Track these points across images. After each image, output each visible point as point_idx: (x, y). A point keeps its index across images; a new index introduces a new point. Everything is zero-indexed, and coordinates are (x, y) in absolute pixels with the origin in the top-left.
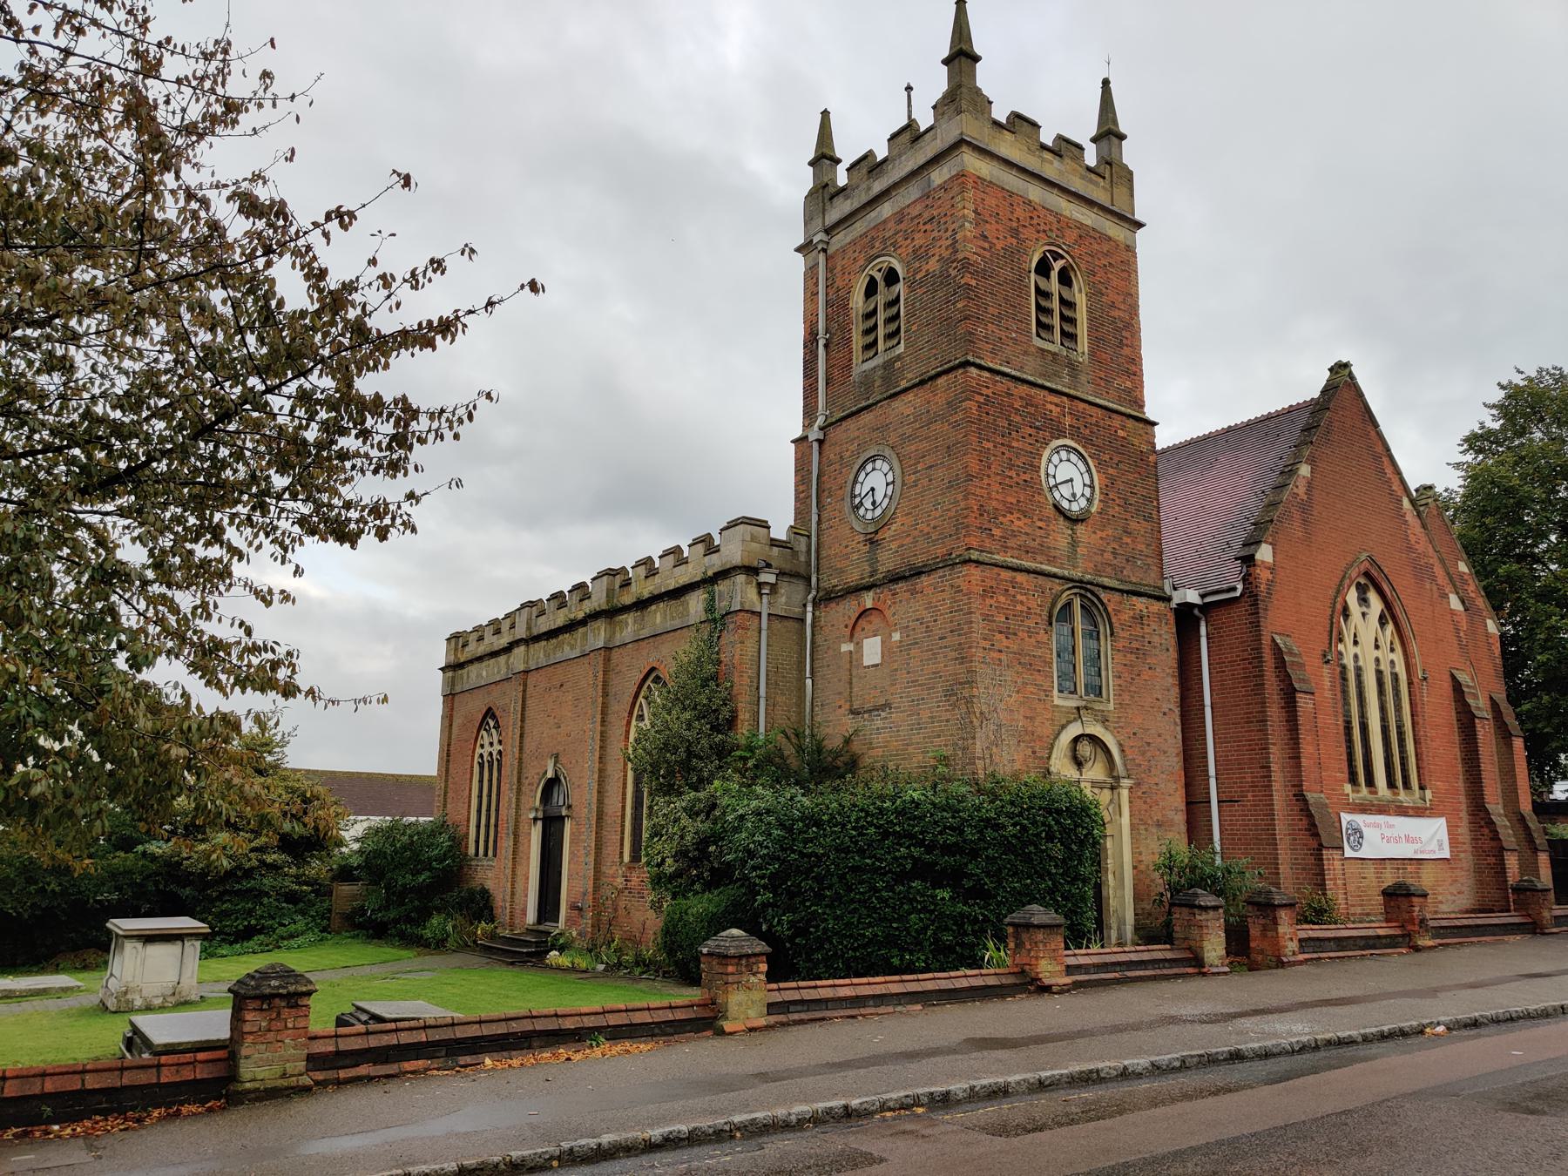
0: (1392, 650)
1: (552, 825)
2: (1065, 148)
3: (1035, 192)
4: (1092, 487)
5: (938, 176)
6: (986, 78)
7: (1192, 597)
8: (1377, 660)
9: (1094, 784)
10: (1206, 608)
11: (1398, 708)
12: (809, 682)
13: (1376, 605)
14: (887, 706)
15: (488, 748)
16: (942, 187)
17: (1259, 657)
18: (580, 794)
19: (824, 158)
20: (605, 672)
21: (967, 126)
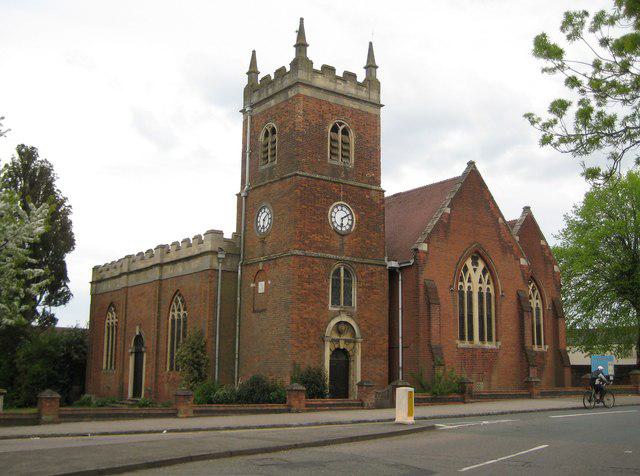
0: (488, 283)
1: (138, 355)
2: (349, 76)
3: (332, 99)
4: (352, 220)
5: (291, 94)
6: (311, 54)
7: (394, 264)
8: (480, 288)
9: (346, 341)
10: (401, 269)
11: (489, 308)
12: (239, 299)
13: (481, 265)
14: (264, 310)
15: (176, 312)
16: (291, 98)
17: (418, 290)
18: (149, 343)
19: (253, 71)
20: (160, 291)
21: (302, 75)
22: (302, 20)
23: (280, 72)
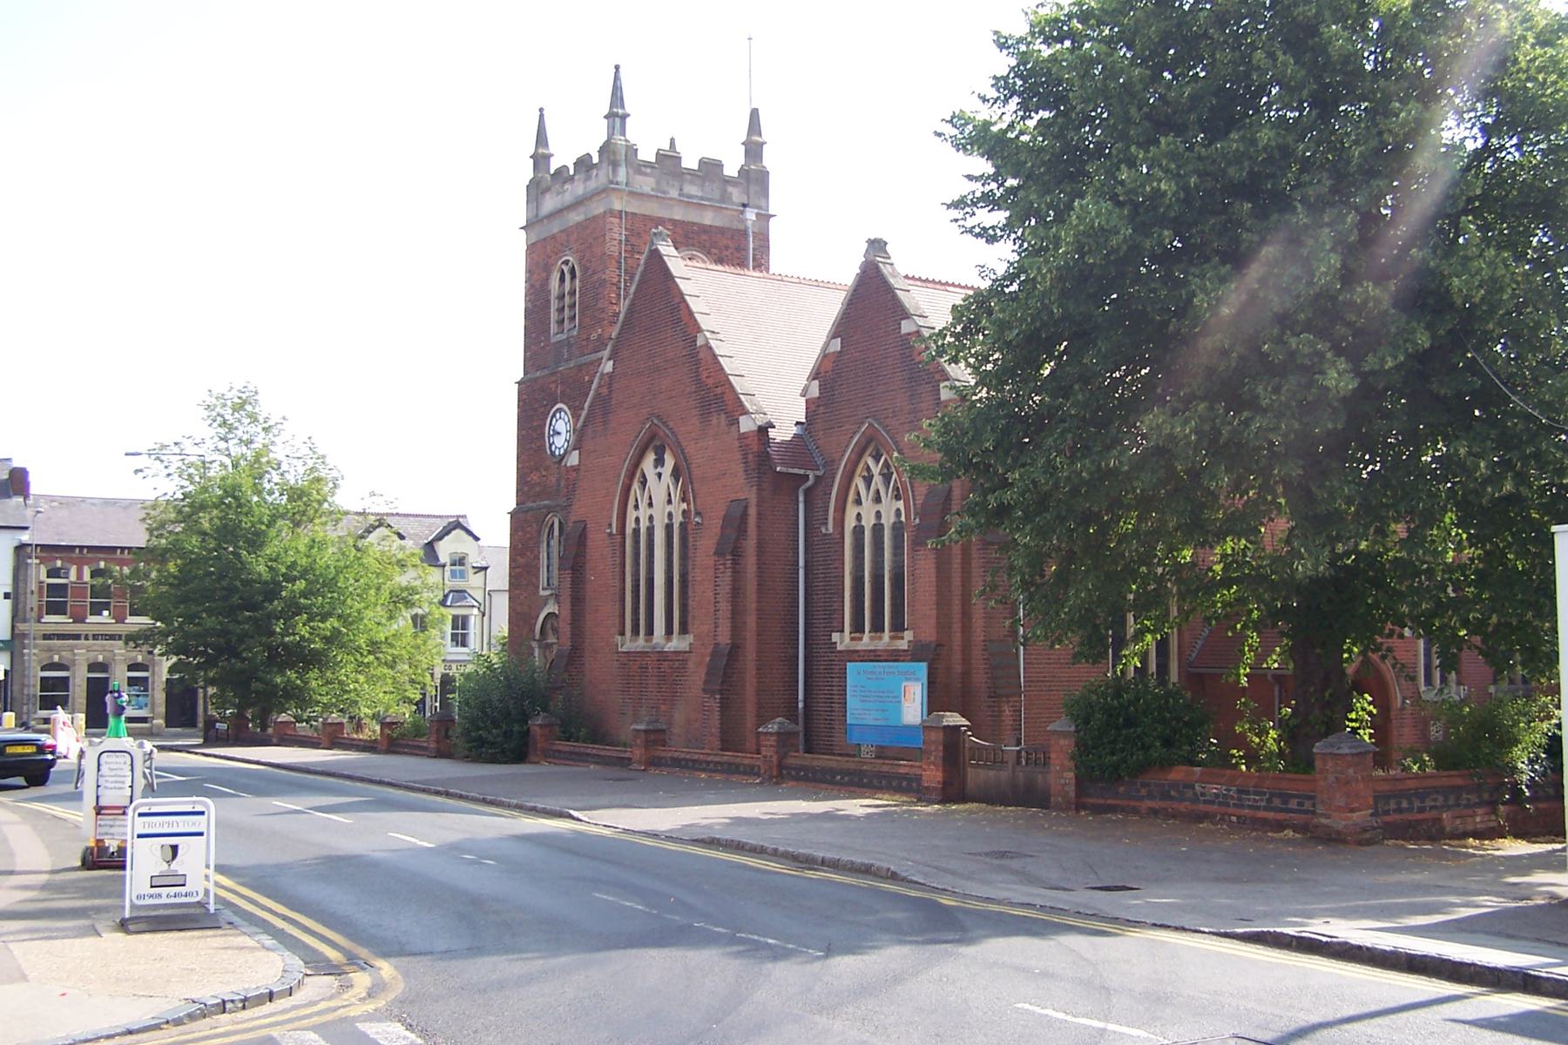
2: (710, 168)
19: (540, 159)
22: (541, 110)
23: (583, 163)
